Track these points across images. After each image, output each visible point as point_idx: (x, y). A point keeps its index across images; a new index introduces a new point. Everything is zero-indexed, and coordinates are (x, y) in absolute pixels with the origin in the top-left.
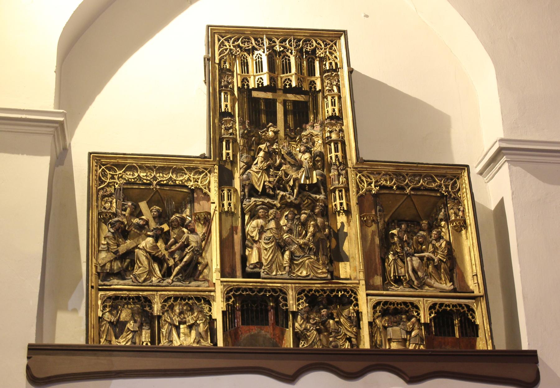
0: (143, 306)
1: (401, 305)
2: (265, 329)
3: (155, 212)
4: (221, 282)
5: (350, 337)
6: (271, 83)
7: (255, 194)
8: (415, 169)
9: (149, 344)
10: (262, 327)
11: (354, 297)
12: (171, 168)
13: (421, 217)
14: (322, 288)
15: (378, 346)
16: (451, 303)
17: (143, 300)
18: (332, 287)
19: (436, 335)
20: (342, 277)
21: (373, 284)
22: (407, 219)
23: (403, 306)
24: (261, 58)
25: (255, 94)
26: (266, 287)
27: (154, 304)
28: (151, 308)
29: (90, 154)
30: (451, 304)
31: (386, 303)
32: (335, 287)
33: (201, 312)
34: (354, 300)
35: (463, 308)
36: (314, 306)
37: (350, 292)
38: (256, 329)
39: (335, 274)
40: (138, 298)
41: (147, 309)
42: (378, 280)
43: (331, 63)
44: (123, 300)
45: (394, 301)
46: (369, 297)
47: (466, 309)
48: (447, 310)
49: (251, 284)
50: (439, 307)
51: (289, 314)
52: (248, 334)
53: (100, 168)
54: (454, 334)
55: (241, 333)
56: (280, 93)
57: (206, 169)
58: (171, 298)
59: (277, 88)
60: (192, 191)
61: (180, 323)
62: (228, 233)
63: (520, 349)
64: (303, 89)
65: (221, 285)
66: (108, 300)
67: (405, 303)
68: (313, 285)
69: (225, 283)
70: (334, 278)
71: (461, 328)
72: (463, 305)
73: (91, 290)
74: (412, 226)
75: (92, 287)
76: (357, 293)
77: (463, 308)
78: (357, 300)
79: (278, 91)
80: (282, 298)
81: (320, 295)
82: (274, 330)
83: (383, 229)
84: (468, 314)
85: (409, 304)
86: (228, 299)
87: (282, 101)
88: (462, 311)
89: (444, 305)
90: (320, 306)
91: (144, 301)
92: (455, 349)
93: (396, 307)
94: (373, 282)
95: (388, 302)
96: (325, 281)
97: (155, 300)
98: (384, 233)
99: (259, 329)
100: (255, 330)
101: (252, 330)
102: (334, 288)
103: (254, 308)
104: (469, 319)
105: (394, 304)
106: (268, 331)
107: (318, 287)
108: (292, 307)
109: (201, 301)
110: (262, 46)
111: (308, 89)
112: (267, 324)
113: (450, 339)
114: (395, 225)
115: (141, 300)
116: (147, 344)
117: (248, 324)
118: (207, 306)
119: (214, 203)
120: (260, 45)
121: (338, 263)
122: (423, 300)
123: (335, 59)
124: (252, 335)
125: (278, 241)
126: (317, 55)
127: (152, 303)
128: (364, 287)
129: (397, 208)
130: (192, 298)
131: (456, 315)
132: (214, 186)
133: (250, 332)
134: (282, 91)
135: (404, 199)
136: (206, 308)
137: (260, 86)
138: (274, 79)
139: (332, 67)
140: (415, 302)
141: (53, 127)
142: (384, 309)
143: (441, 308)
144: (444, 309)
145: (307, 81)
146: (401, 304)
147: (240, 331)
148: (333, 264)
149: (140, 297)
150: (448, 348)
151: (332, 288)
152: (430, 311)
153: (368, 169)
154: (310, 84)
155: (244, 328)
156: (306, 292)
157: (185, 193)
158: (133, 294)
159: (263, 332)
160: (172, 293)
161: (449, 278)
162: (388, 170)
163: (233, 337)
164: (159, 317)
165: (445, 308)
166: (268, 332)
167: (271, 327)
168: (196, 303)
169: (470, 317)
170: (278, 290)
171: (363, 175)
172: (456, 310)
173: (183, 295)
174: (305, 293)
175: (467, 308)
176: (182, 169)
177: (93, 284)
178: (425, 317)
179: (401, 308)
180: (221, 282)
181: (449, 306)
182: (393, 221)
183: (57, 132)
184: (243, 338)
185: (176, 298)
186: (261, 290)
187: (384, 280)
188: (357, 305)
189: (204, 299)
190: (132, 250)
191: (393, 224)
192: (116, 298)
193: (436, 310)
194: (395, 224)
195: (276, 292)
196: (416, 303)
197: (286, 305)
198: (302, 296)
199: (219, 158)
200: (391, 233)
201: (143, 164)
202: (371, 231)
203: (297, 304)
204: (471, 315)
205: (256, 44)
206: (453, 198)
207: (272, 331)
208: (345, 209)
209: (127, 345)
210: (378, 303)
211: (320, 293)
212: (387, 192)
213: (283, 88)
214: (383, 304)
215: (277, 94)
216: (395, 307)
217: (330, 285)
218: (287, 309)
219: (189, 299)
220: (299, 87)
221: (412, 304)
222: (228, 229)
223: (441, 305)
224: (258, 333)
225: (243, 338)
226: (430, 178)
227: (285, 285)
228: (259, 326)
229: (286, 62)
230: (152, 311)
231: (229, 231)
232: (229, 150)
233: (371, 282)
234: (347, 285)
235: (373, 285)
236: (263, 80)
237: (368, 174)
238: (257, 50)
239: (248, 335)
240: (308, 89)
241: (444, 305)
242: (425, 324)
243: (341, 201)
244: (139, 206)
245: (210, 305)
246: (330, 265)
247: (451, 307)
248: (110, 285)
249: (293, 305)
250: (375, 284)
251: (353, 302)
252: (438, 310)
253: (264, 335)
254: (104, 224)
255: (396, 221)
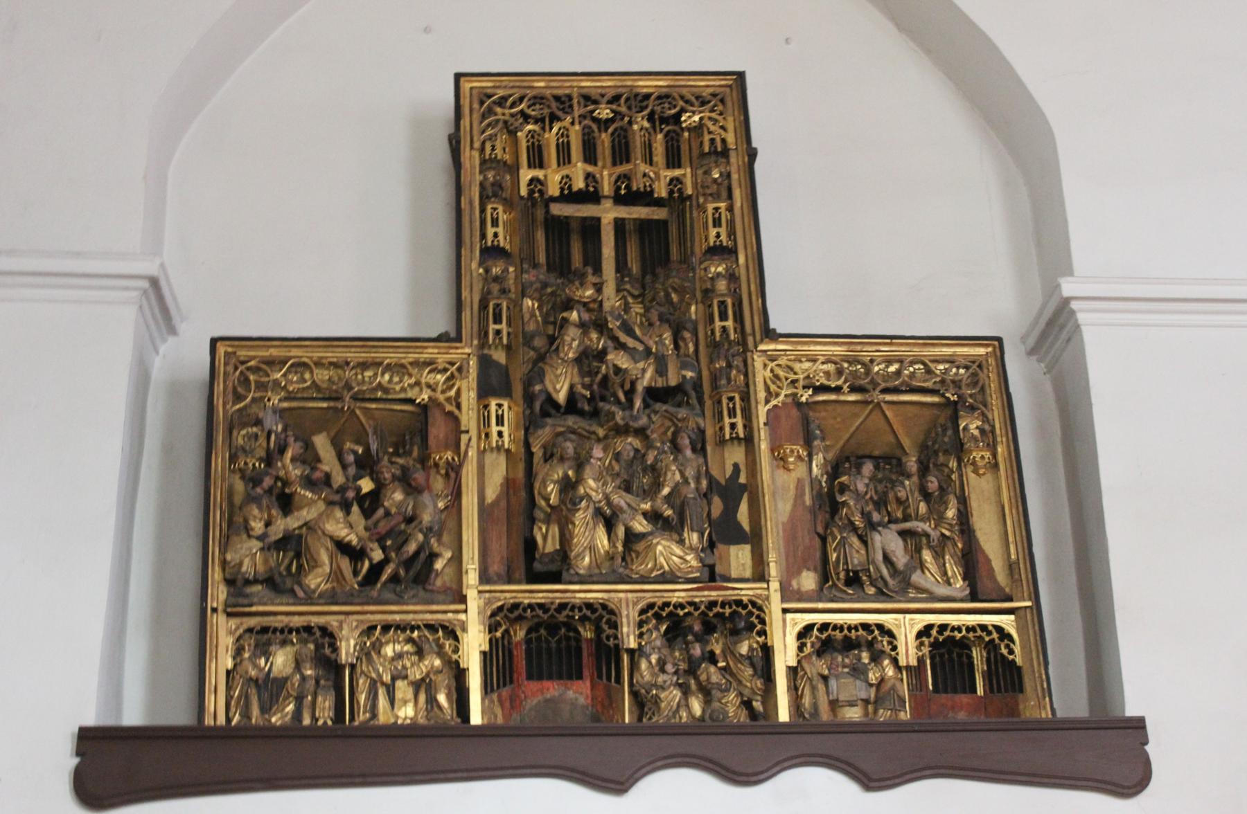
0: (319, 647)
1: (857, 630)
2: (574, 688)
3: (250, 446)
4: (480, 592)
5: (748, 698)
6: (587, 186)
7: (553, 412)
8: (903, 349)
9: (330, 723)
10: (569, 682)
11: (758, 617)
12: (380, 364)
13: (906, 449)
14: (689, 600)
15: (807, 716)
16: (964, 623)
17: (318, 634)
18: (711, 596)
19: (936, 689)
20: (734, 575)
21: (799, 589)
22: (876, 453)
23: (861, 632)
24: (568, 136)
25: (557, 210)
26: (573, 600)
27: (341, 642)
28: (335, 649)
30: (964, 625)
31: (824, 627)
32: (718, 596)
33: (440, 653)
34: (756, 621)
35: (989, 633)
36: (675, 638)
37: (750, 606)
38: (556, 687)
39: (718, 569)
40: (308, 629)
41: (327, 651)
42: (808, 581)
43: (712, 141)
44: (278, 633)
45: (841, 622)
46: (789, 616)
47: (995, 635)
48: (954, 637)
49: (541, 595)
50: (937, 632)
51: (621, 653)
52: (540, 698)
53: (236, 368)
54: (974, 690)
55: (525, 697)
56: (608, 204)
57: (452, 364)
58: (374, 628)
59: (601, 194)
60: (424, 408)
61: (394, 679)
62: (497, 493)
63: (1121, 715)
64: (656, 195)
65: (480, 598)
66: (247, 635)
67: (866, 627)
68: (670, 594)
69: (487, 595)
70: (718, 578)
71: (989, 676)
72: (990, 628)
73: (212, 616)
74: (887, 467)
76: (764, 608)
77: (989, 633)
78: (763, 622)
79: (603, 201)
80: (607, 623)
81: (686, 614)
82: (593, 687)
83: (822, 475)
84: (1000, 645)
85: (874, 627)
86: (492, 629)
87: (612, 221)
88: (987, 639)
89: (949, 628)
90: (687, 636)
91: (321, 636)
92: (975, 719)
93: (846, 636)
94: (798, 584)
95: (829, 624)
96: (695, 586)
97: (344, 632)
98: (826, 482)
99: (563, 688)
100: (553, 689)
101: (548, 689)
102: (715, 598)
103: (554, 645)
104: (1002, 655)
105: (841, 628)
106: (580, 690)
107: (683, 598)
108: (626, 640)
109: (438, 631)
110: (569, 110)
111: (664, 194)
112: (580, 677)
113: (964, 699)
114: (850, 467)
115: (314, 634)
116: (325, 723)
117: (540, 678)
118: (451, 641)
119: (467, 432)
120: (567, 110)
121: (726, 547)
122: (904, 618)
123: (721, 131)
124: (547, 701)
125: (597, 505)
126: (684, 125)
127: (335, 639)
128: (778, 595)
129: (854, 432)
130: (418, 627)
131: (978, 649)
132: (469, 397)
133: (543, 693)
134: (611, 201)
135: (867, 412)
136: (448, 645)
137: (566, 192)
138: (594, 177)
139: (716, 147)
140: (886, 624)
141: (135, 289)
142: (821, 638)
143: (942, 635)
144: (949, 636)
145: (662, 178)
146: (856, 628)
147: (523, 692)
148: (715, 550)
149: (312, 628)
150: (962, 716)
151: (712, 599)
152: (918, 641)
153: (788, 353)
154: (669, 185)
155: (531, 686)
156: (656, 608)
157: (401, 414)
159: (571, 694)
160: (378, 617)
161: (961, 572)
162: (831, 353)
163: (507, 704)
164: (353, 667)
165: (952, 634)
166: (581, 693)
167: (588, 683)
168: (426, 636)
169: (1004, 651)
170: (599, 606)
171: (779, 365)
172: (974, 637)
173: (400, 620)
174: (654, 611)
175: (997, 632)
176: (403, 366)
177: (215, 605)
178: (908, 651)
179: (857, 637)
180: (480, 592)
181: (959, 629)
182: (847, 459)
183: (148, 298)
184: (527, 707)
185: (386, 628)
186: (562, 606)
187: (825, 577)
188: (763, 633)
189: (444, 628)
191: (847, 465)
192: (265, 630)
193: (932, 640)
194: (850, 464)
195: (594, 611)
196: (888, 626)
197: (616, 638)
198: (648, 617)
199: (479, 341)
200: (839, 482)
201: (322, 358)
202: (796, 480)
203: (637, 633)
204: (1007, 646)
205: (558, 108)
206: (968, 406)
207: (589, 692)
208: (742, 435)
210: (808, 629)
211: (686, 610)
212: (833, 397)
213: (613, 194)
214: (818, 630)
215: (601, 207)
216: (843, 634)
217: (706, 593)
218: (617, 646)
219: (413, 629)
220: (645, 190)
221: (880, 627)
222: (498, 484)
223: (943, 627)
224: (560, 695)
225: (527, 707)
226: (922, 367)
227: (613, 595)
228: (562, 682)
229: (620, 142)
230: (337, 655)
231: (499, 488)
232: (501, 322)
233: (794, 584)
234: (743, 592)
235: (799, 591)
236: (570, 180)
237: (790, 363)
238: (559, 119)
239: (539, 701)
240: (664, 194)
241: (949, 628)
242: (908, 668)
243: (733, 420)
244: (313, 444)
245: (456, 639)
246: (708, 551)
247: (964, 632)
248: (251, 605)
249: (628, 636)
250: (803, 589)
251: (756, 626)
252: (936, 639)
253: (571, 699)
255: (852, 459)
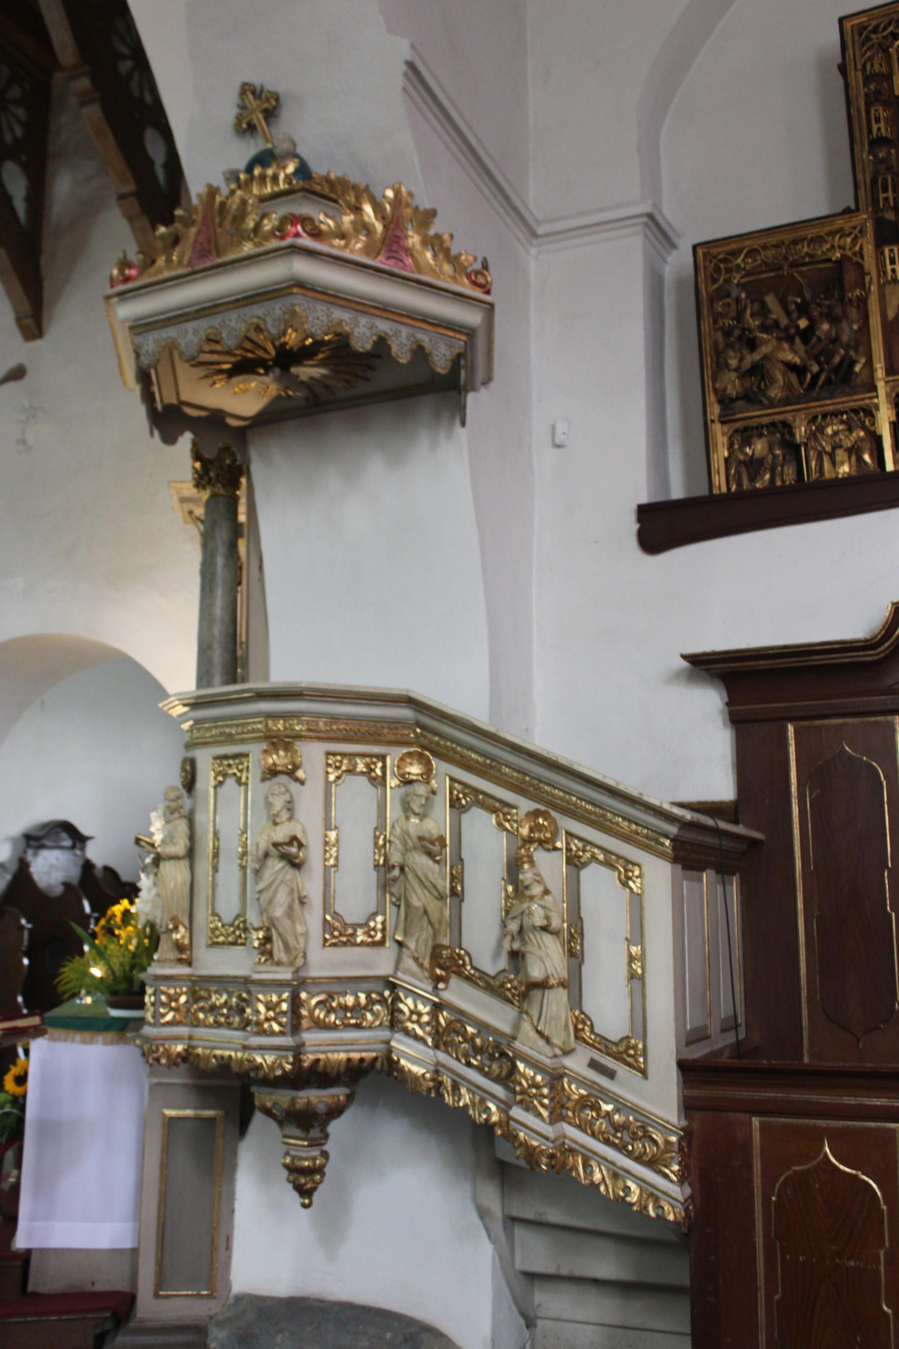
17: (780, 426)
27: (795, 428)
28: (792, 435)
29: (695, 248)
40: (773, 424)
41: (787, 437)
53: (711, 261)
75: (713, 421)
158: (766, 420)
177: (713, 418)
190: (761, 362)
192: (746, 429)
209: (430, 1044)
254: (395, 349)
